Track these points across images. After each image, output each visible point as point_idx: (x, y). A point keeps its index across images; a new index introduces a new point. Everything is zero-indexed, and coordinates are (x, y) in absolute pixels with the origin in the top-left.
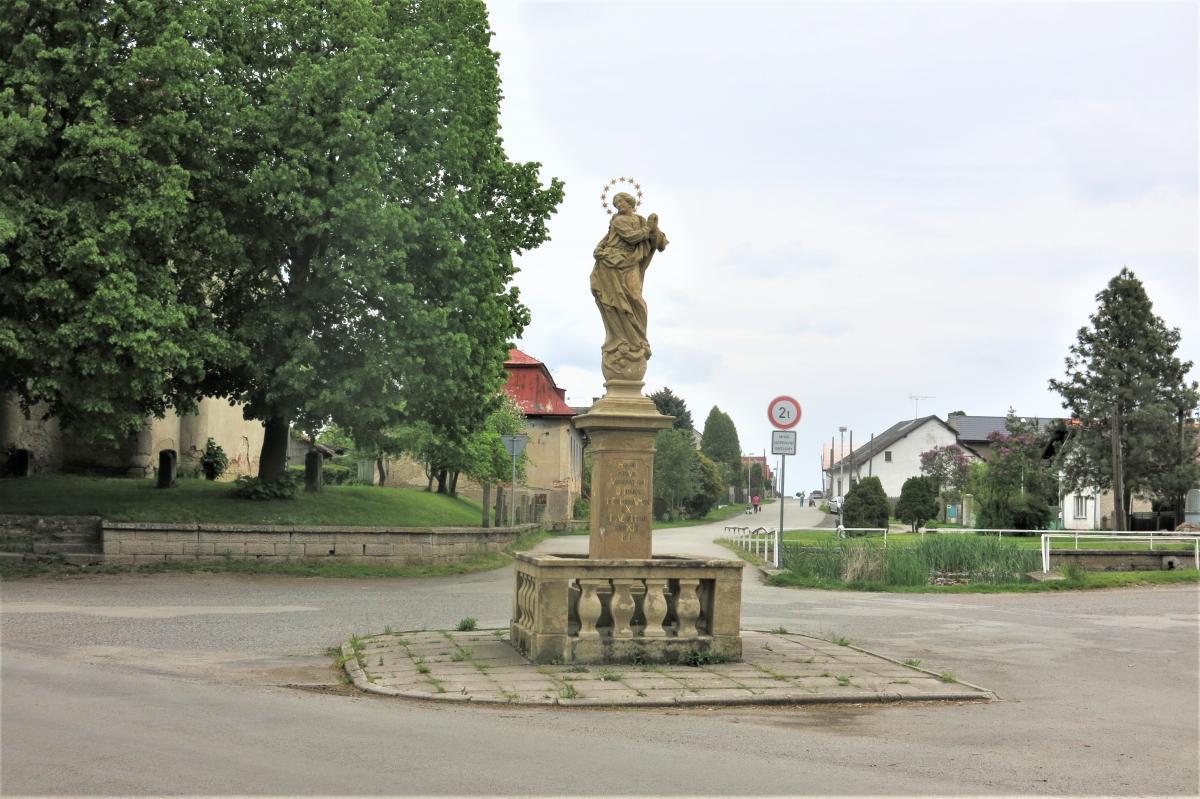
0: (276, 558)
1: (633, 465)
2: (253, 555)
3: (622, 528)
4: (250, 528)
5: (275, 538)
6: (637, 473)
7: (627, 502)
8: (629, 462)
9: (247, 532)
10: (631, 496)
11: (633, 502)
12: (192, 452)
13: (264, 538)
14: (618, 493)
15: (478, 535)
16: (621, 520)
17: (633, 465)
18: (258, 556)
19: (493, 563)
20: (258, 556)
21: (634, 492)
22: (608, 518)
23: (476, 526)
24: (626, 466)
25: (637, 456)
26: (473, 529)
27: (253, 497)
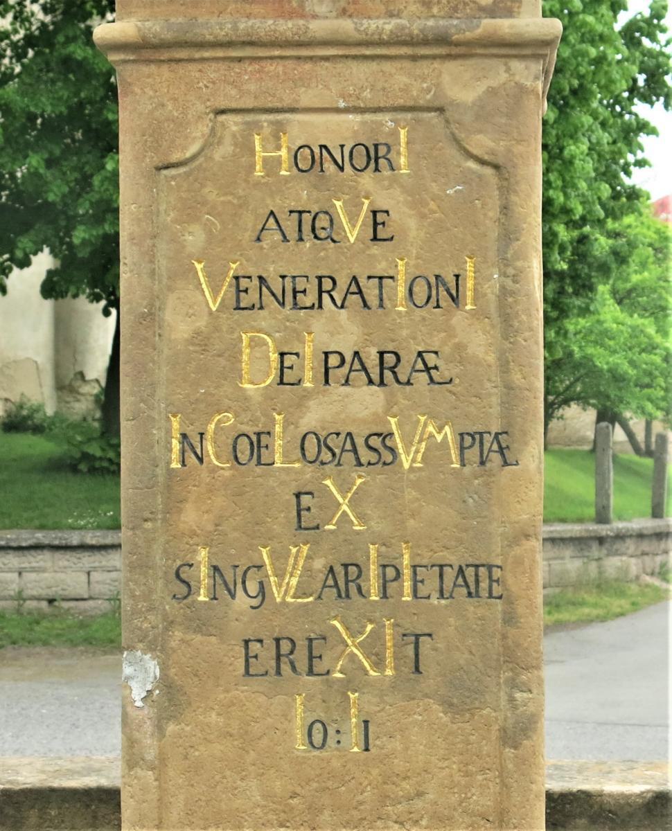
0: (91, 603)
1: (374, 156)
2: (39, 599)
3: (290, 655)
4: (27, 537)
5: (88, 560)
6: (403, 218)
7: (325, 448)
8: (341, 130)
9: (20, 548)
10: (361, 404)
11: (378, 448)
12: (78, 383)
13: (63, 559)
14: (256, 381)
15: (579, 542)
16: (284, 590)
17: (374, 156)
18: (51, 601)
19: (617, 604)
20: (51, 601)
21: (385, 369)
22: (182, 580)
23: (580, 520)
24: (312, 160)
25: (402, 80)
26: (575, 529)
27: (83, 467)
